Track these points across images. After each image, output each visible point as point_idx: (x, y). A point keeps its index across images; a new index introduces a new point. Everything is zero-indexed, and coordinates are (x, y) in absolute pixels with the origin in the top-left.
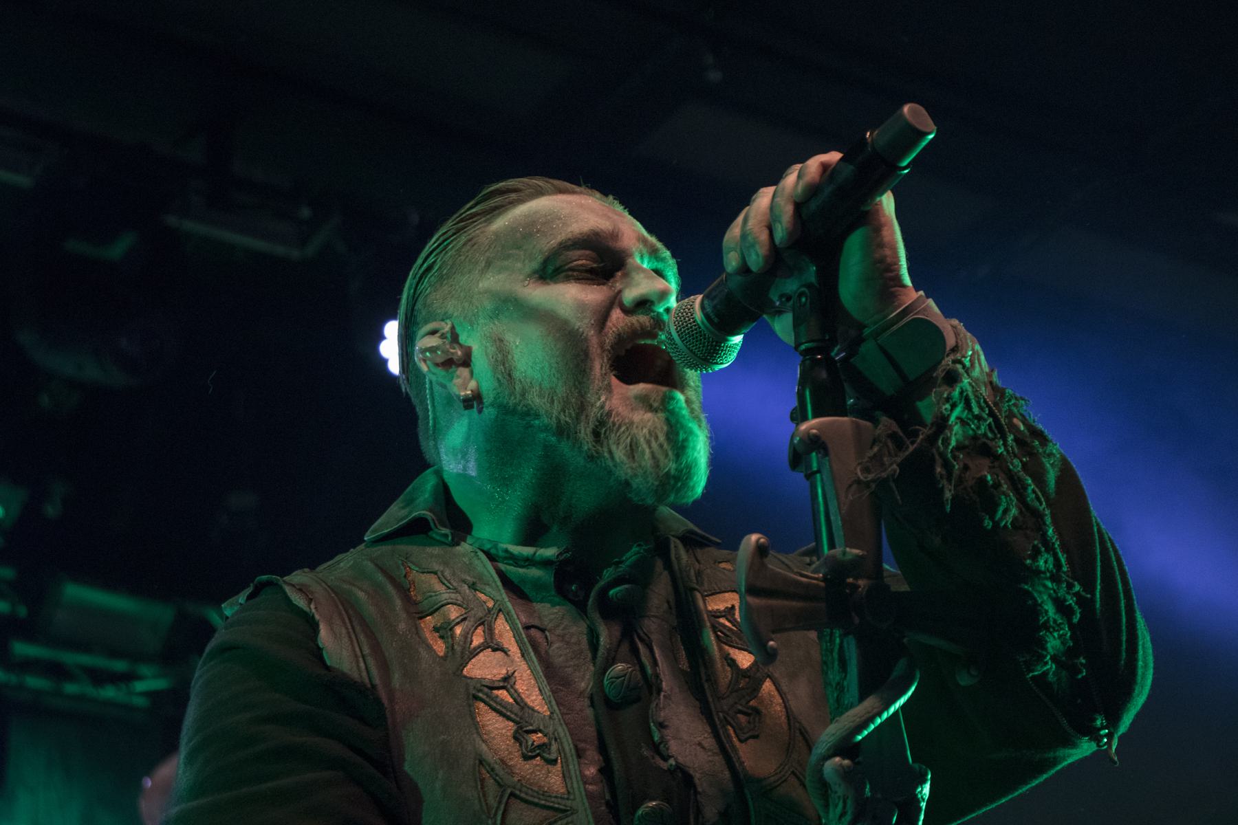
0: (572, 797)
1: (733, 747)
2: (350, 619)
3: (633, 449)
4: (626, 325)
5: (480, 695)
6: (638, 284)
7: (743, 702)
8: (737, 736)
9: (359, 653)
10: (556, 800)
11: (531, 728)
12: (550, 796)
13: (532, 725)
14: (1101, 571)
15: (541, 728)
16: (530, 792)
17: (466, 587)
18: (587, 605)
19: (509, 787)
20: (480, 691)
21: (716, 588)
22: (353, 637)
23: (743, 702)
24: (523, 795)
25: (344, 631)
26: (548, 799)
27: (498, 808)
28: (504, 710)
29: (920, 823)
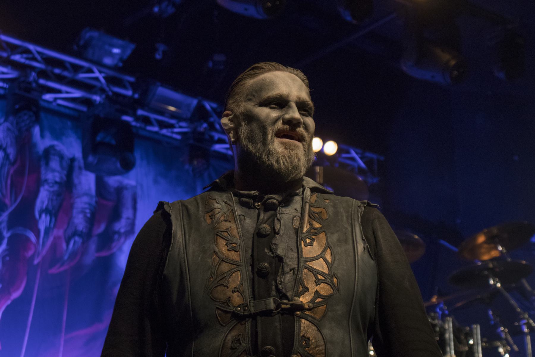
0: (241, 262)
1: (301, 248)
2: (183, 215)
3: (278, 161)
4: (287, 92)
5: (218, 234)
6: (289, 113)
7: (310, 236)
8: (304, 244)
9: (182, 224)
10: (236, 262)
11: (232, 242)
12: (234, 261)
13: (233, 241)
14: (245, 191)
15: (236, 242)
16: (228, 260)
17: (224, 203)
18: (268, 195)
19: (222, 258)
20: (218, 233)
21: (319, 206)
22: (182, 220)
23: (310, 236)
24: (226, 261)
25: (179, 218)
26: (234, 262)
27: (217, 264)
28: (225, 238)
29: (481, 355)
